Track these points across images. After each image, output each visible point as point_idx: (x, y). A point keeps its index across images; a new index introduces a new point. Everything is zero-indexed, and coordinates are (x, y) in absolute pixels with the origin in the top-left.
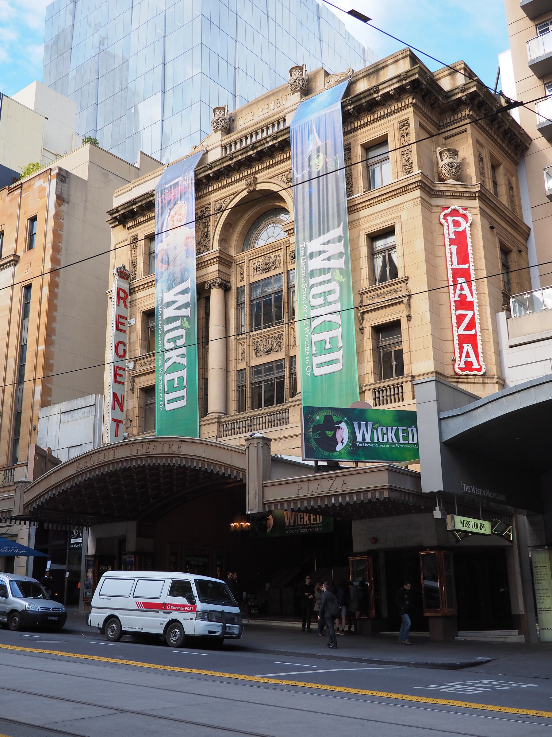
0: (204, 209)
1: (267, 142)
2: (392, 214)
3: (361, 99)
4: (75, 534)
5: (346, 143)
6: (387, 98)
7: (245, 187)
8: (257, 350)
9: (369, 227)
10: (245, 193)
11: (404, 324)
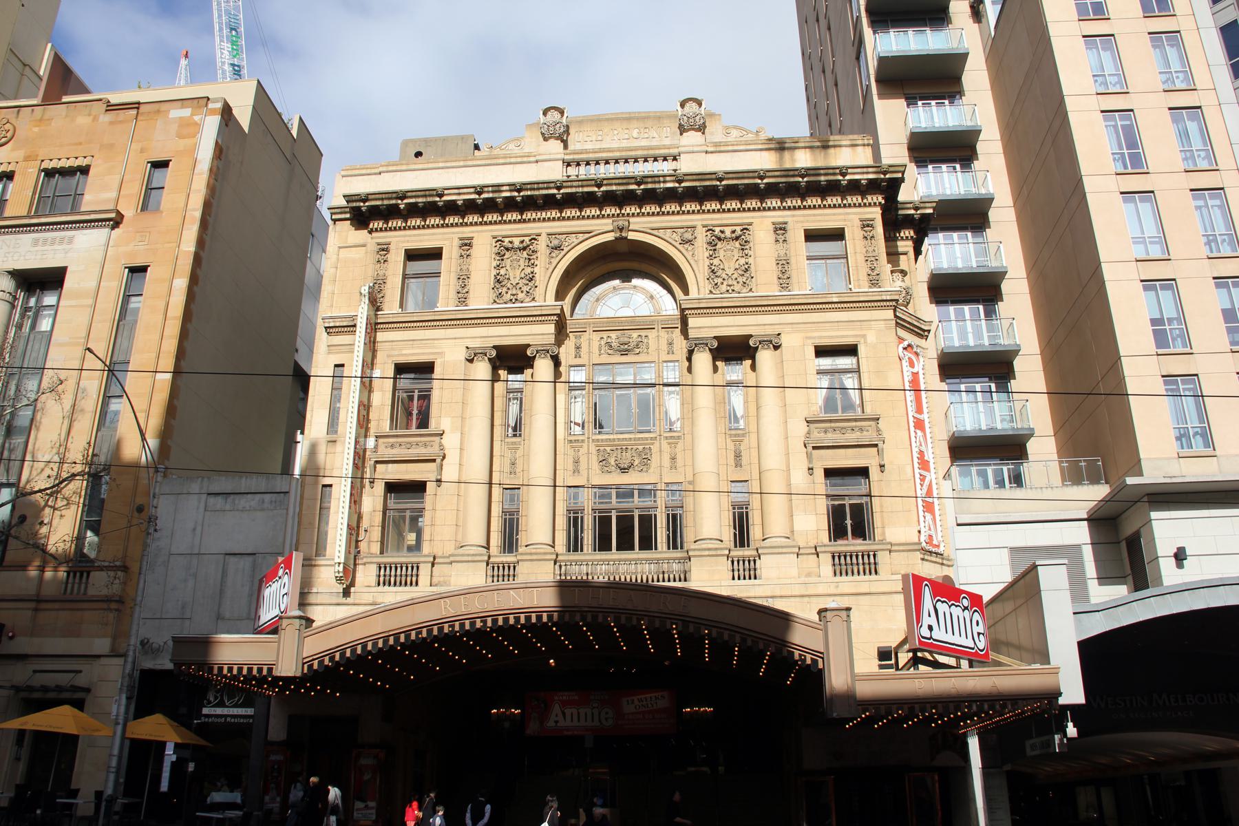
0: (527, 239)
1: (665, 182)
2: (853, 329)
3: (820, 175)
4: (212, 699)
5: (188, 142)
6: (855, 188)
7: (611, 228)
8: (603, 461)
9: (820, 337)
10: (610, 237)
11: (430, 487)
